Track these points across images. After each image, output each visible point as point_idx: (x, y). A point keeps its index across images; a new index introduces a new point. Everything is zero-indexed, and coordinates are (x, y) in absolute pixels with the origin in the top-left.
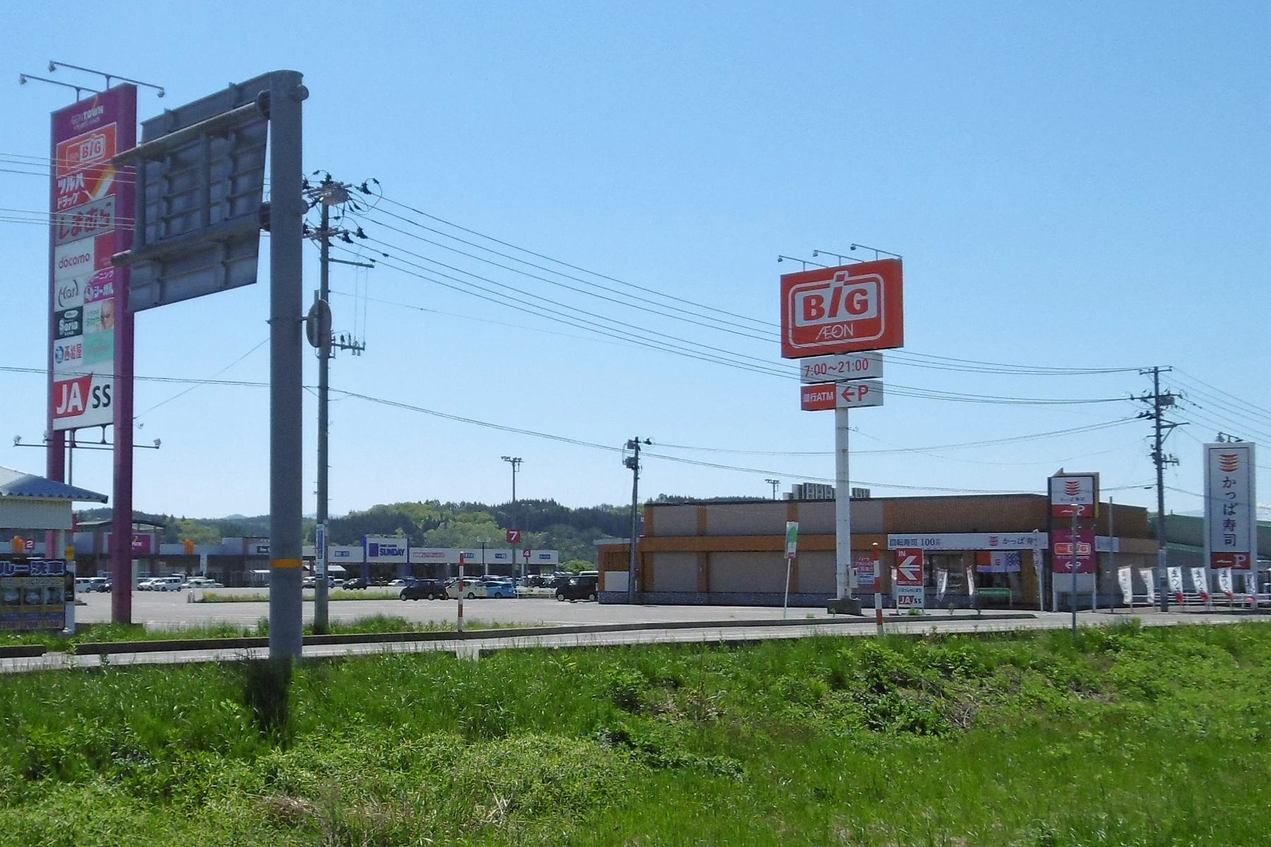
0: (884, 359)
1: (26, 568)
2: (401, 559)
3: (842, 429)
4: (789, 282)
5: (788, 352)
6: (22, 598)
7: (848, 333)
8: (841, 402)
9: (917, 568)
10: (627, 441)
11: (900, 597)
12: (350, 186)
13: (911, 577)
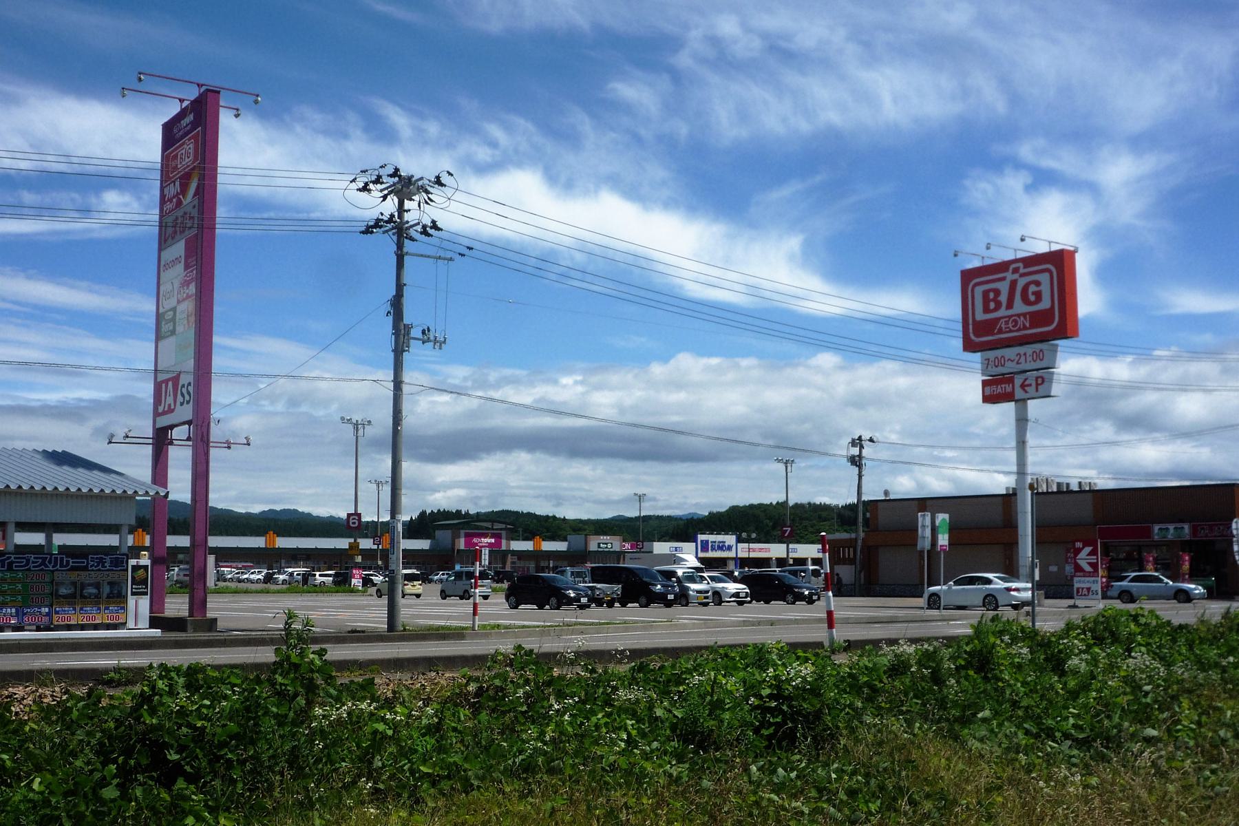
0: (1059, 348)
1: (84, 563)
2: (732, 554)
3: (1022, 421)
4: (968, 276)
5: (969, 346)
6: (78, 592)
7: (1024, 325)
8: (1019, 393)
9: (1093, 559)
10: (850, 440)
11: (1078, 589)
12: (421, 179)
13: (1088, 568)
